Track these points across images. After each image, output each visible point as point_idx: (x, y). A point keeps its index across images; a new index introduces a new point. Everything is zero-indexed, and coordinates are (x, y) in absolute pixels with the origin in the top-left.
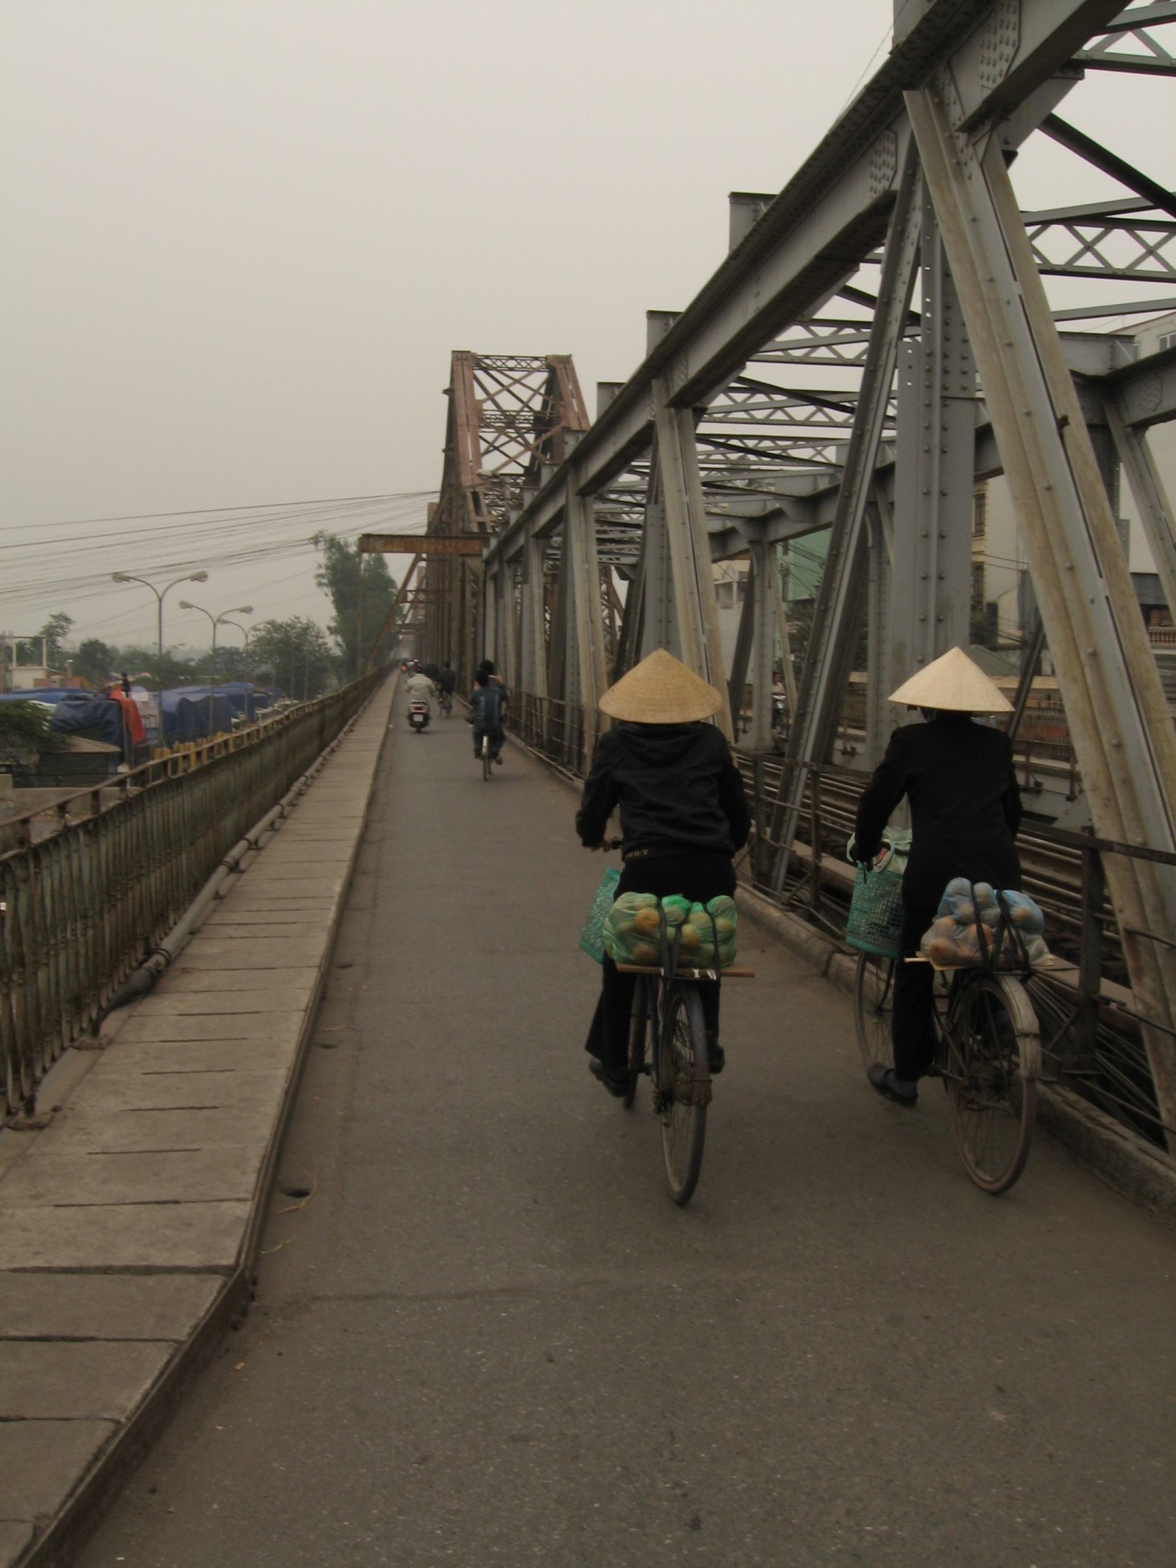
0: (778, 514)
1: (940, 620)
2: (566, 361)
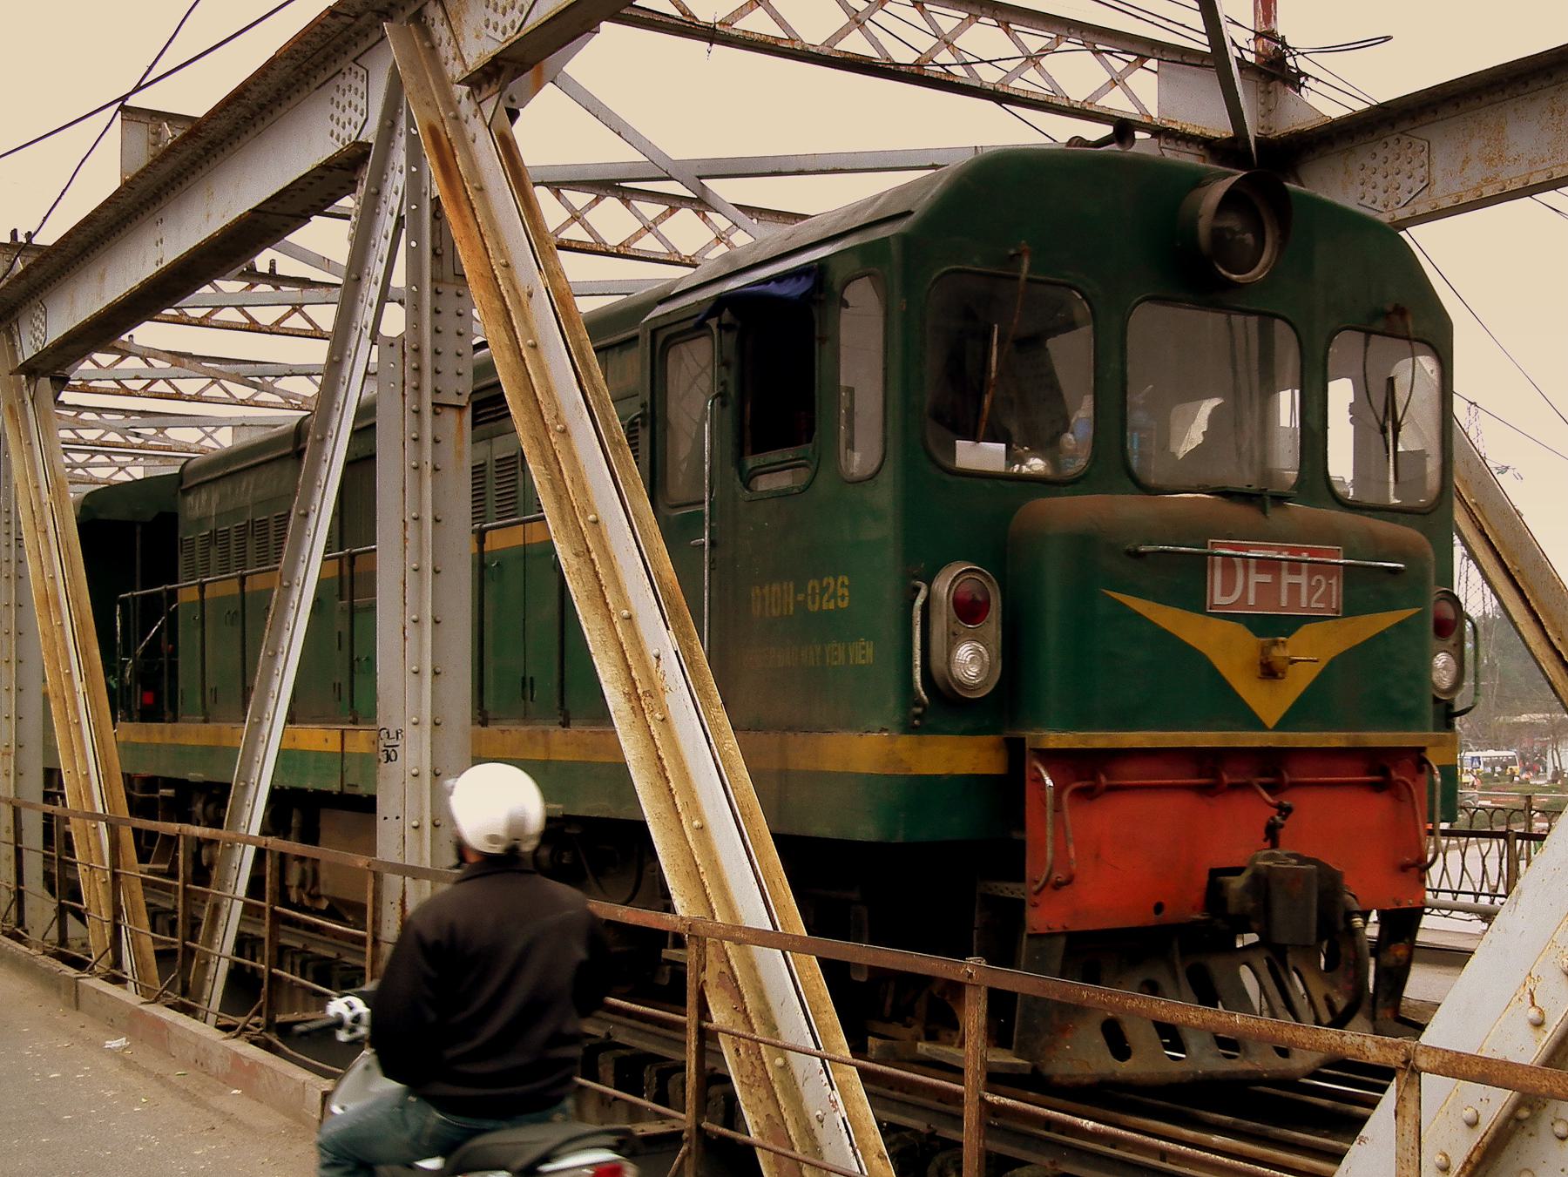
1: (437, 775)
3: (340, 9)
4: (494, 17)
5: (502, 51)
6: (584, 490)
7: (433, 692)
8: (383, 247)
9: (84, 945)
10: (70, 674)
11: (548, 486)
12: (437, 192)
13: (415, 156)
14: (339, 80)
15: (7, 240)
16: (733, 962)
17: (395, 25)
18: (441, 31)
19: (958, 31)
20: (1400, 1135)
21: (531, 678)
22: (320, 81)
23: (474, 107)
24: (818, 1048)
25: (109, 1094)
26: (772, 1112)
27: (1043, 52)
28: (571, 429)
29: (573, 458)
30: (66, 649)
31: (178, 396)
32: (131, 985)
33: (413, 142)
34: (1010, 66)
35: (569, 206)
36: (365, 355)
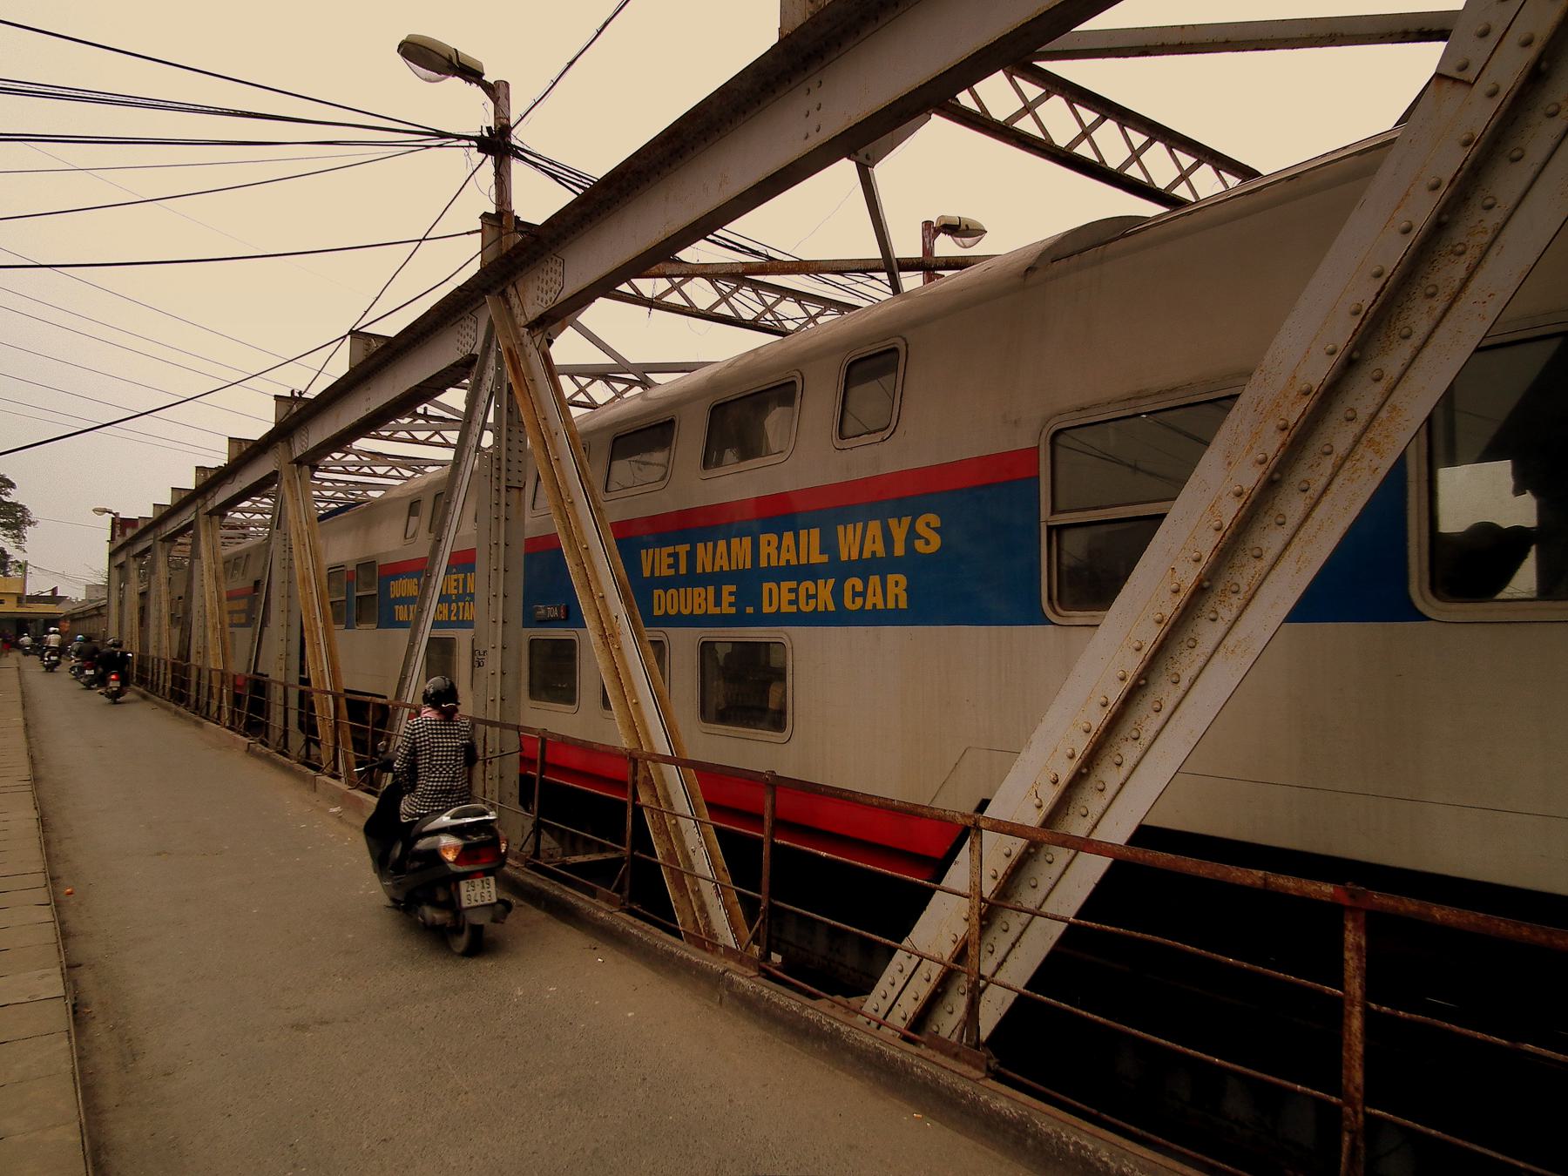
3: (463, 287)
4: (541, 295)
5: (546, 312)
6: (582, 532)
7: (503, 631)
8: (483, 406)
9: (318, 758)
10: (315, 618)
11: (563, 530)
12: (511, 381)
13: (500, 362)
14: (462, 322)
15: (290, 395)
16: (651, 771)
17: (490, 297)
18: (514, 301)
20: (971, 860)
22: (453, 322)
23: (530, 338)
24: (693, 815)
25: (332, 836)
26: (669, 847)
27: (818, 315)
28: (575, 501)
29: (576, 516)
30: (314, 606)
31: (375, 475)
32: (343, 779)
33: (499, 355)
34: (801, 321)
35: (578, 384)
36: (472, 462)
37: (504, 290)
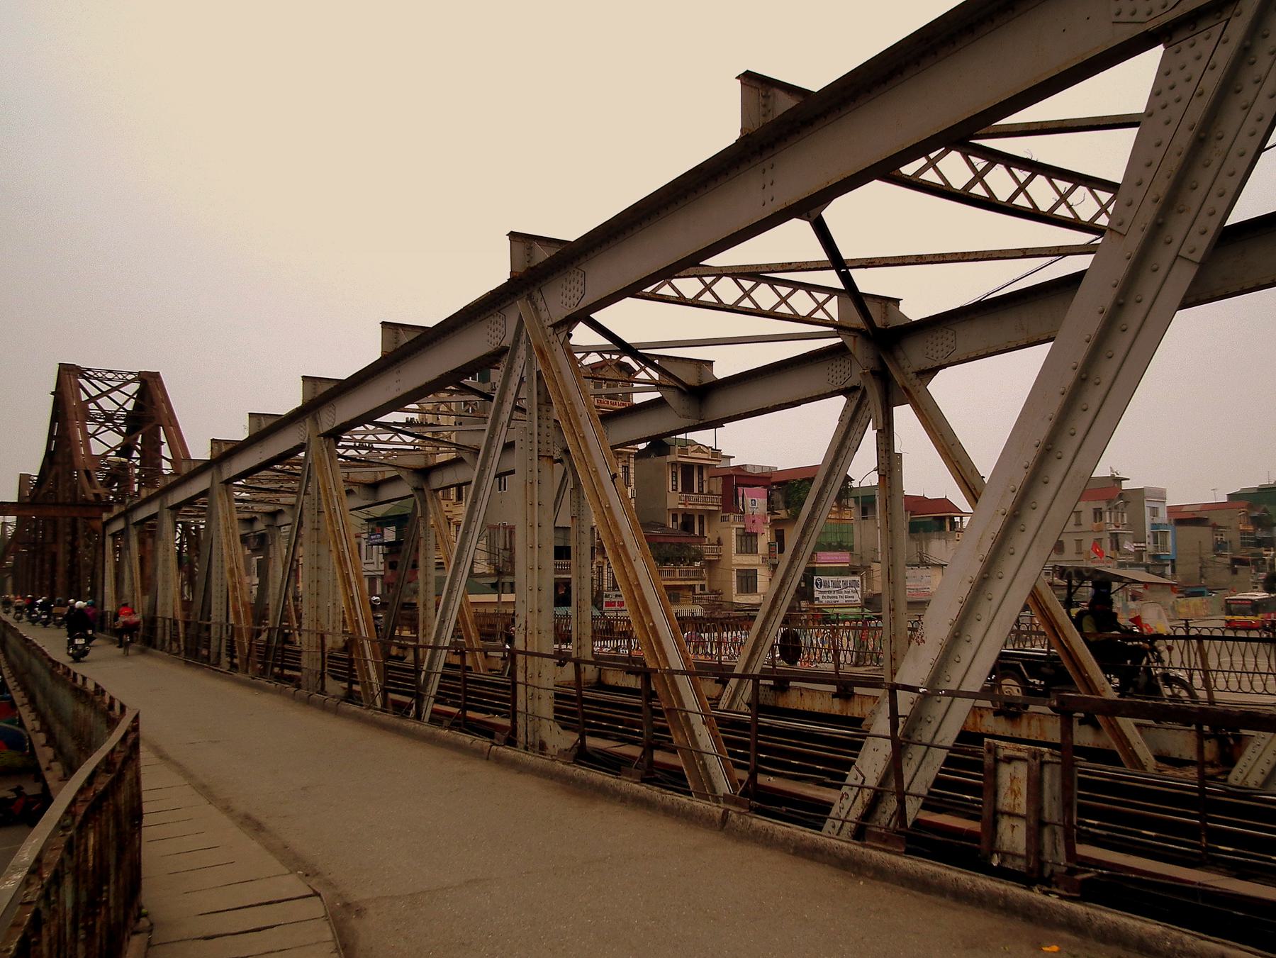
0: (280, 512)
2: (157, 375)
13: (530, 354)
18: (541, 305)
19: (752, 289)
21: (555, 686)
37: (531, 293)
